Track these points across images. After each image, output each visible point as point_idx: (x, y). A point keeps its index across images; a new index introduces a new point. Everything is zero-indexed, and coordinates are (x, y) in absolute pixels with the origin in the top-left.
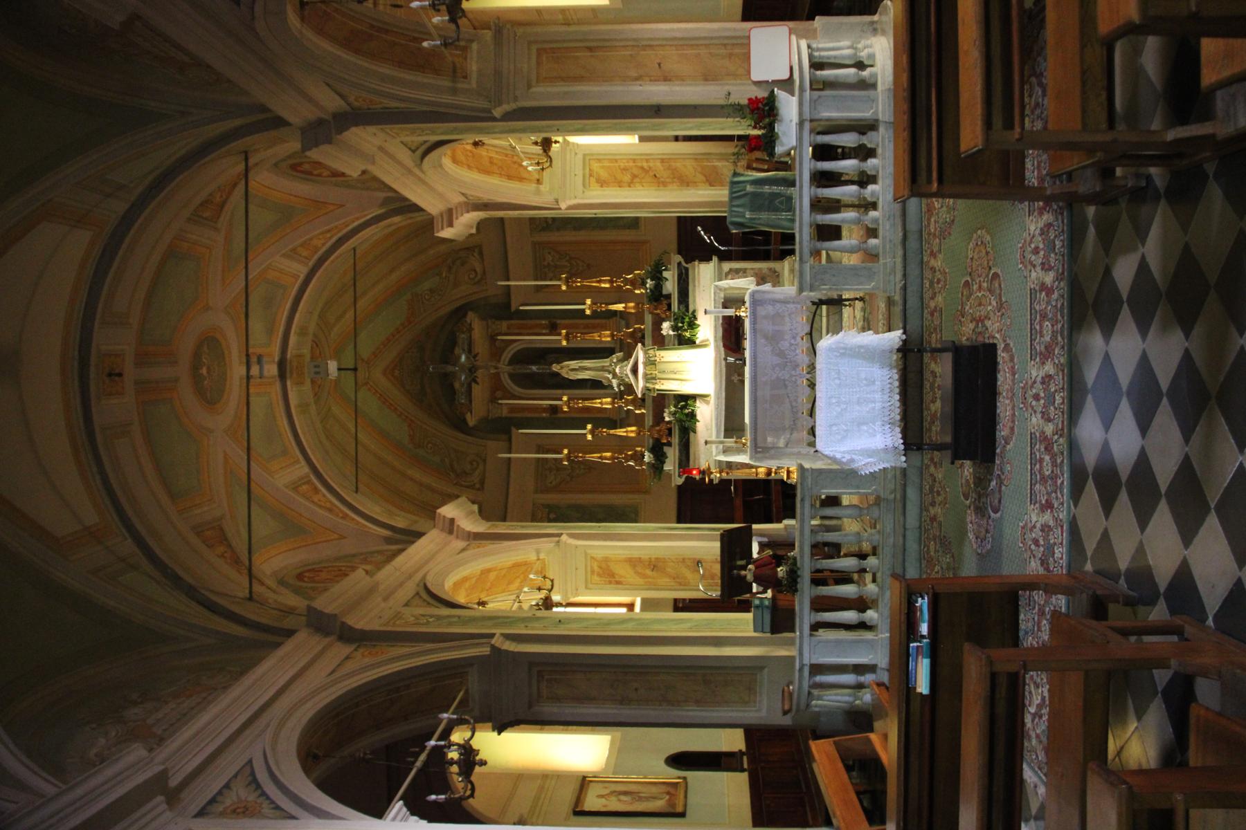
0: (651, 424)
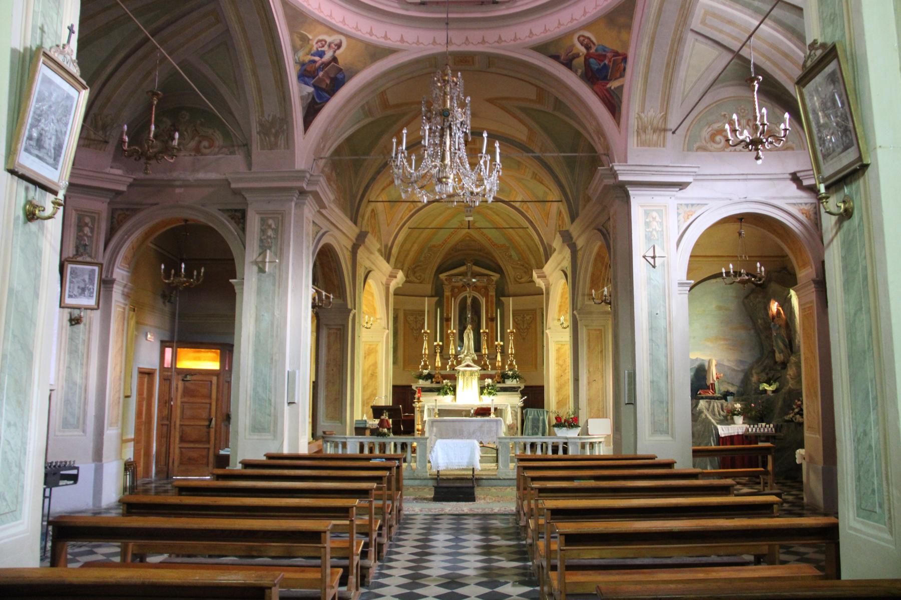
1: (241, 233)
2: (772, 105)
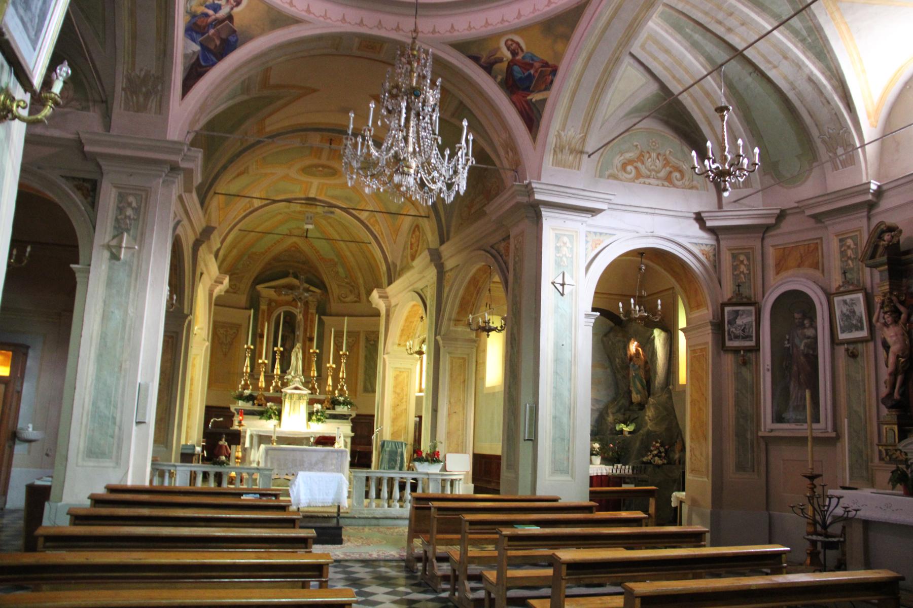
0: (266, 395)
1: (89, 208)
2: (681, 142)
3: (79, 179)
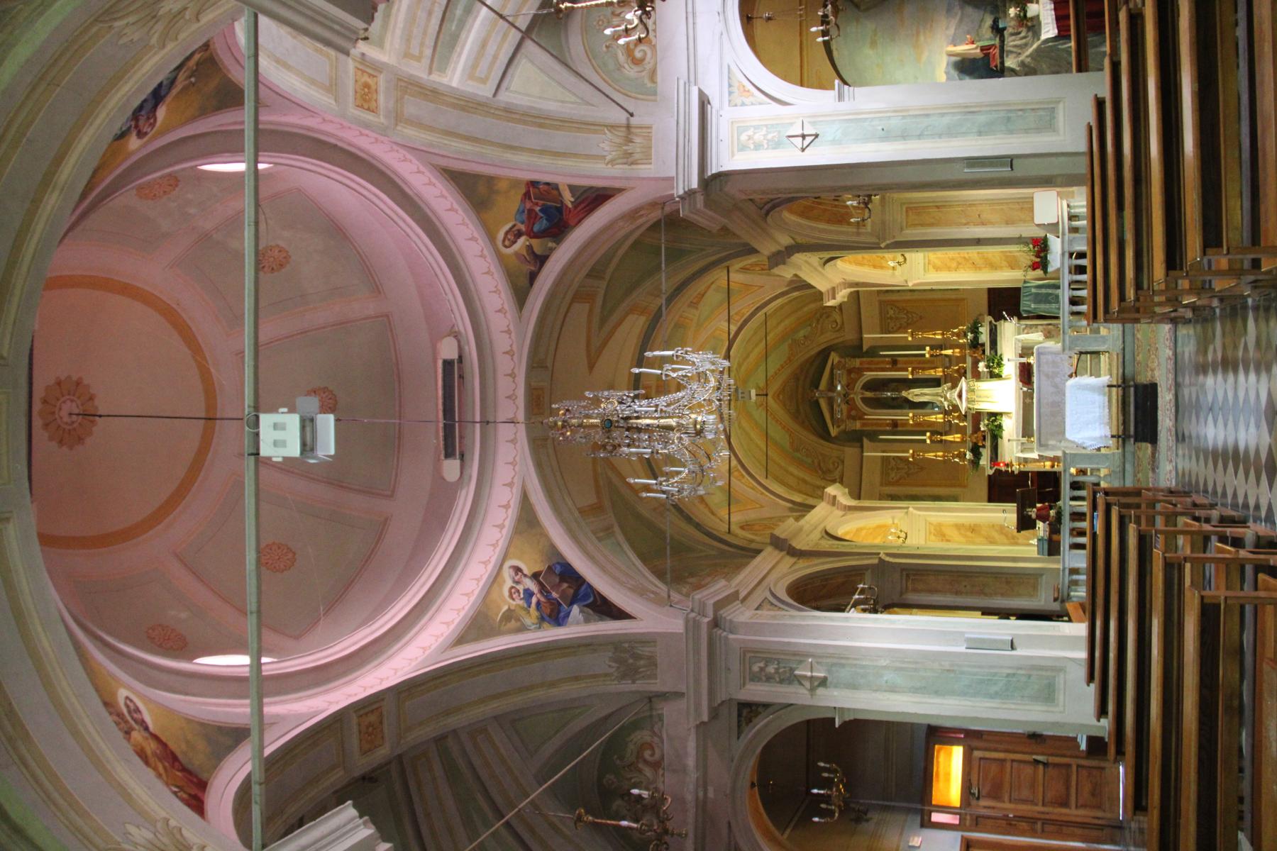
1: (771, 710)
3: (739, 721)
